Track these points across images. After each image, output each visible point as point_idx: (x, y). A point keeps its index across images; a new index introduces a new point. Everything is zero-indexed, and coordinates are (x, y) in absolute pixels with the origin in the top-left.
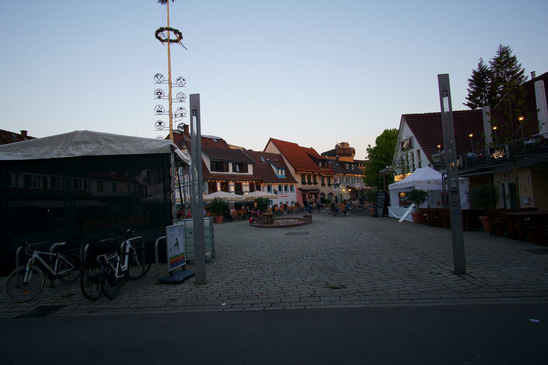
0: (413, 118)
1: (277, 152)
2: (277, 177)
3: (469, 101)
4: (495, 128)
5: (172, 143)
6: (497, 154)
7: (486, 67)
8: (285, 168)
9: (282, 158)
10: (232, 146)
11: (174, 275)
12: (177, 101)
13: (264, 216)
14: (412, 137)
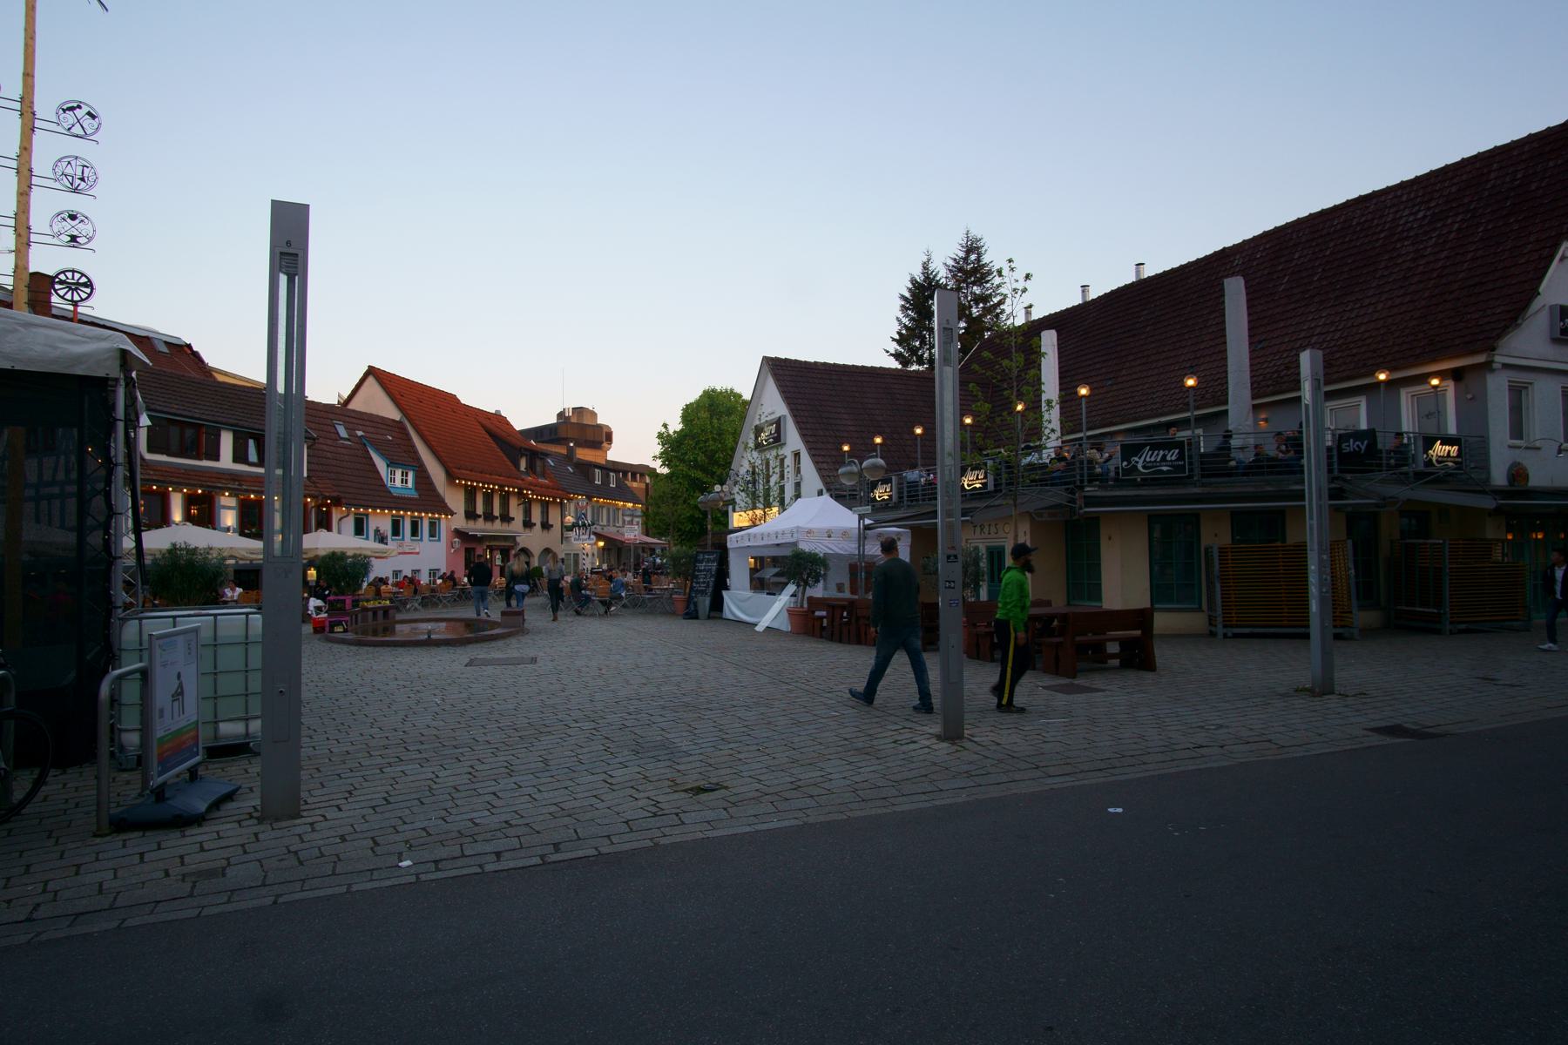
1: (390, 412)
2: (390, 492)
3: (898, 348)
4: (968, 421)
5: (130, 346)
6: (1148, 459)
7: (936, 275)
8: (415, 464)
9: (408, 434)
10: (226, 374)
11: (168, 799)
12: (57, 185)
13: (365, 609)
14: (785, 416)
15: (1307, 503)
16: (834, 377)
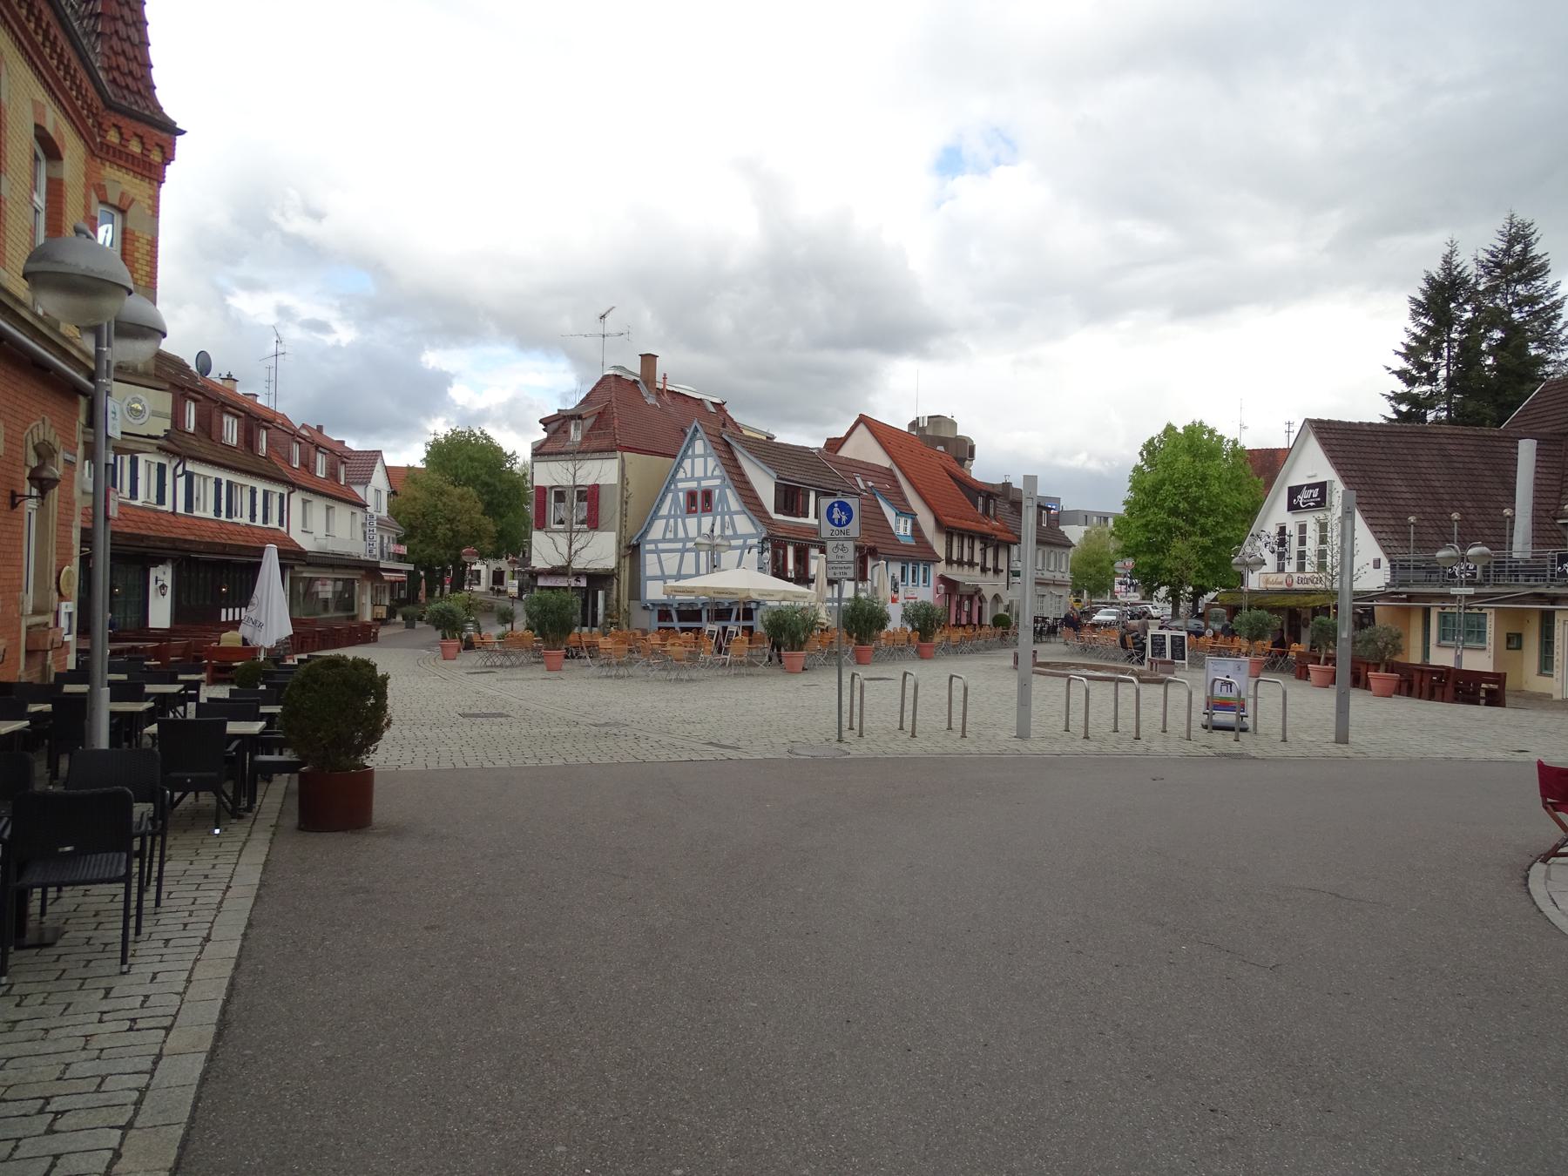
0: (1334, 431)
14: (1332, 482)
16: (1383, 439)
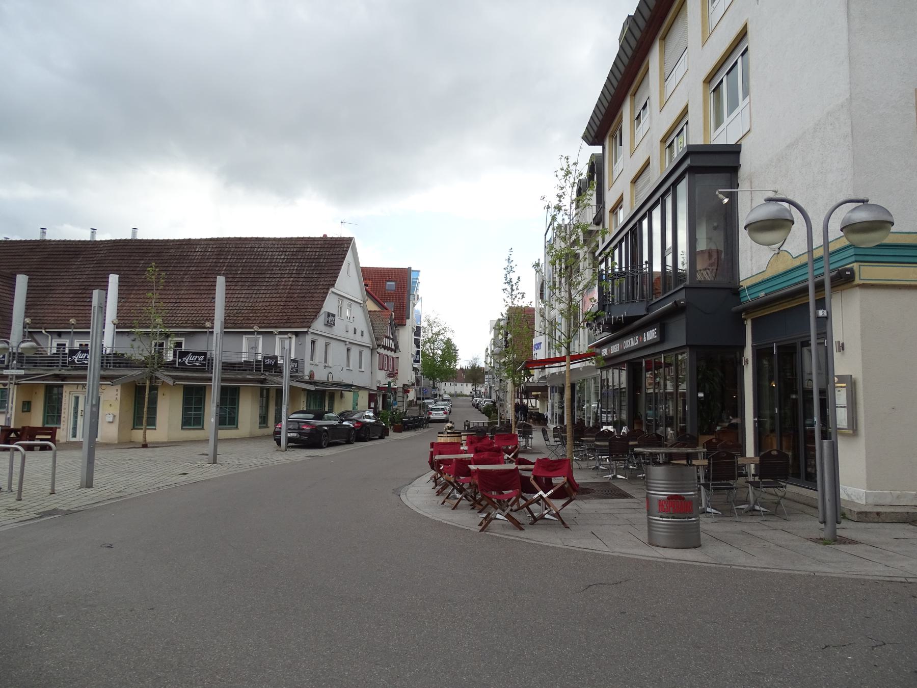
6: (190, 359)
15: (213, 384)
